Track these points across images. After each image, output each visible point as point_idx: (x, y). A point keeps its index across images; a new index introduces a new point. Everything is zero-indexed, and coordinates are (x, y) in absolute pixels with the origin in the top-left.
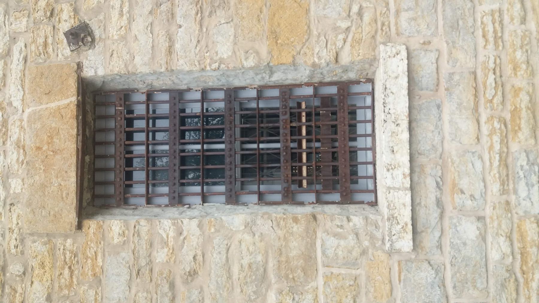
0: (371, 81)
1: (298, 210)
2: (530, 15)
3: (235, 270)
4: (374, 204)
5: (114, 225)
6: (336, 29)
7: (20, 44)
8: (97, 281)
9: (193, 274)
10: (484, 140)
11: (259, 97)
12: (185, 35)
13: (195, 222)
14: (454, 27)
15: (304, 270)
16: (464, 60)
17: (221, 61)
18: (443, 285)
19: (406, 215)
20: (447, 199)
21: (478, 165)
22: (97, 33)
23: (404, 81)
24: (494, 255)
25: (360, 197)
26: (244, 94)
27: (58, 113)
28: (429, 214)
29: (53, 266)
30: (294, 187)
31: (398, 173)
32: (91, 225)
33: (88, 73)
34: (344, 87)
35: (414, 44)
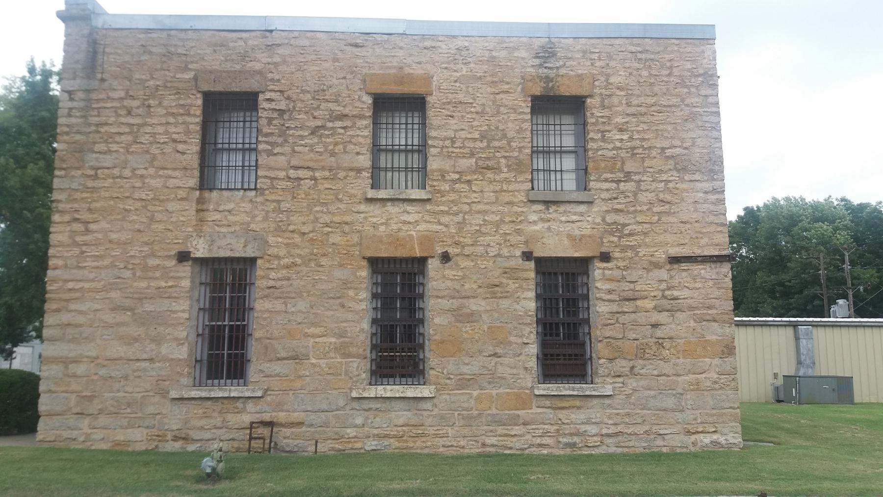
0: (424, 384)
1: (369, 351)
2: (446, 449)
3: (344, 324)
4: (370, 384)
5: (364, 273)
6: (443, 368)
7: (444, 229)
8: (341, 265)
9: (343, 306)
10: (396, 428)
11: (420, 334)
12: (445, 304)
13: (364, 307)
14: (442, 418)
15: (344, 353)
16: (428, 421)
17: (433, 319)
18: (338, 410)
19: (366, 395)
20: (372, 412)
21: (385, 425)
22: (447, 265)
23: (419, 395)
24: (349, 431)
25: (374, 379)
26: (421, 326)
27: (413, 248)
28: (366, 405)
29: (347, 246)
30: (379, 349)
31: (383, 392)
32: (365, 263)
33: (430, 261)
34: (422, 373)
35: (435, 400)
